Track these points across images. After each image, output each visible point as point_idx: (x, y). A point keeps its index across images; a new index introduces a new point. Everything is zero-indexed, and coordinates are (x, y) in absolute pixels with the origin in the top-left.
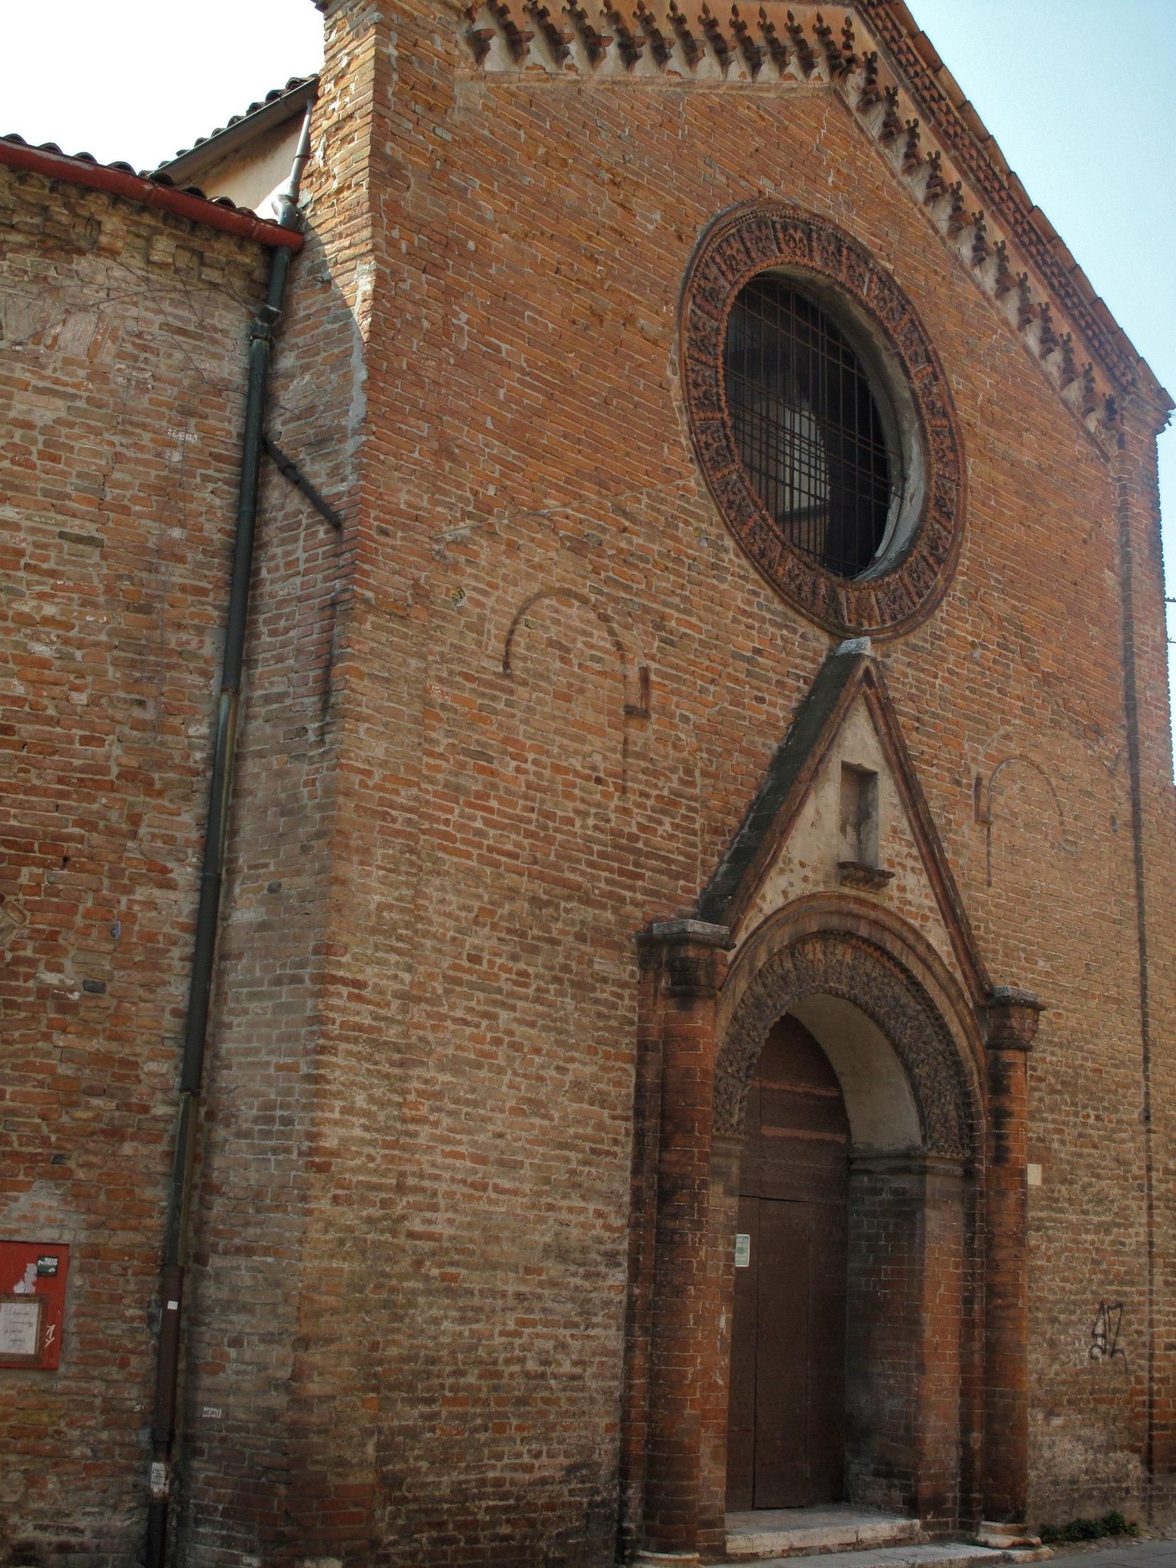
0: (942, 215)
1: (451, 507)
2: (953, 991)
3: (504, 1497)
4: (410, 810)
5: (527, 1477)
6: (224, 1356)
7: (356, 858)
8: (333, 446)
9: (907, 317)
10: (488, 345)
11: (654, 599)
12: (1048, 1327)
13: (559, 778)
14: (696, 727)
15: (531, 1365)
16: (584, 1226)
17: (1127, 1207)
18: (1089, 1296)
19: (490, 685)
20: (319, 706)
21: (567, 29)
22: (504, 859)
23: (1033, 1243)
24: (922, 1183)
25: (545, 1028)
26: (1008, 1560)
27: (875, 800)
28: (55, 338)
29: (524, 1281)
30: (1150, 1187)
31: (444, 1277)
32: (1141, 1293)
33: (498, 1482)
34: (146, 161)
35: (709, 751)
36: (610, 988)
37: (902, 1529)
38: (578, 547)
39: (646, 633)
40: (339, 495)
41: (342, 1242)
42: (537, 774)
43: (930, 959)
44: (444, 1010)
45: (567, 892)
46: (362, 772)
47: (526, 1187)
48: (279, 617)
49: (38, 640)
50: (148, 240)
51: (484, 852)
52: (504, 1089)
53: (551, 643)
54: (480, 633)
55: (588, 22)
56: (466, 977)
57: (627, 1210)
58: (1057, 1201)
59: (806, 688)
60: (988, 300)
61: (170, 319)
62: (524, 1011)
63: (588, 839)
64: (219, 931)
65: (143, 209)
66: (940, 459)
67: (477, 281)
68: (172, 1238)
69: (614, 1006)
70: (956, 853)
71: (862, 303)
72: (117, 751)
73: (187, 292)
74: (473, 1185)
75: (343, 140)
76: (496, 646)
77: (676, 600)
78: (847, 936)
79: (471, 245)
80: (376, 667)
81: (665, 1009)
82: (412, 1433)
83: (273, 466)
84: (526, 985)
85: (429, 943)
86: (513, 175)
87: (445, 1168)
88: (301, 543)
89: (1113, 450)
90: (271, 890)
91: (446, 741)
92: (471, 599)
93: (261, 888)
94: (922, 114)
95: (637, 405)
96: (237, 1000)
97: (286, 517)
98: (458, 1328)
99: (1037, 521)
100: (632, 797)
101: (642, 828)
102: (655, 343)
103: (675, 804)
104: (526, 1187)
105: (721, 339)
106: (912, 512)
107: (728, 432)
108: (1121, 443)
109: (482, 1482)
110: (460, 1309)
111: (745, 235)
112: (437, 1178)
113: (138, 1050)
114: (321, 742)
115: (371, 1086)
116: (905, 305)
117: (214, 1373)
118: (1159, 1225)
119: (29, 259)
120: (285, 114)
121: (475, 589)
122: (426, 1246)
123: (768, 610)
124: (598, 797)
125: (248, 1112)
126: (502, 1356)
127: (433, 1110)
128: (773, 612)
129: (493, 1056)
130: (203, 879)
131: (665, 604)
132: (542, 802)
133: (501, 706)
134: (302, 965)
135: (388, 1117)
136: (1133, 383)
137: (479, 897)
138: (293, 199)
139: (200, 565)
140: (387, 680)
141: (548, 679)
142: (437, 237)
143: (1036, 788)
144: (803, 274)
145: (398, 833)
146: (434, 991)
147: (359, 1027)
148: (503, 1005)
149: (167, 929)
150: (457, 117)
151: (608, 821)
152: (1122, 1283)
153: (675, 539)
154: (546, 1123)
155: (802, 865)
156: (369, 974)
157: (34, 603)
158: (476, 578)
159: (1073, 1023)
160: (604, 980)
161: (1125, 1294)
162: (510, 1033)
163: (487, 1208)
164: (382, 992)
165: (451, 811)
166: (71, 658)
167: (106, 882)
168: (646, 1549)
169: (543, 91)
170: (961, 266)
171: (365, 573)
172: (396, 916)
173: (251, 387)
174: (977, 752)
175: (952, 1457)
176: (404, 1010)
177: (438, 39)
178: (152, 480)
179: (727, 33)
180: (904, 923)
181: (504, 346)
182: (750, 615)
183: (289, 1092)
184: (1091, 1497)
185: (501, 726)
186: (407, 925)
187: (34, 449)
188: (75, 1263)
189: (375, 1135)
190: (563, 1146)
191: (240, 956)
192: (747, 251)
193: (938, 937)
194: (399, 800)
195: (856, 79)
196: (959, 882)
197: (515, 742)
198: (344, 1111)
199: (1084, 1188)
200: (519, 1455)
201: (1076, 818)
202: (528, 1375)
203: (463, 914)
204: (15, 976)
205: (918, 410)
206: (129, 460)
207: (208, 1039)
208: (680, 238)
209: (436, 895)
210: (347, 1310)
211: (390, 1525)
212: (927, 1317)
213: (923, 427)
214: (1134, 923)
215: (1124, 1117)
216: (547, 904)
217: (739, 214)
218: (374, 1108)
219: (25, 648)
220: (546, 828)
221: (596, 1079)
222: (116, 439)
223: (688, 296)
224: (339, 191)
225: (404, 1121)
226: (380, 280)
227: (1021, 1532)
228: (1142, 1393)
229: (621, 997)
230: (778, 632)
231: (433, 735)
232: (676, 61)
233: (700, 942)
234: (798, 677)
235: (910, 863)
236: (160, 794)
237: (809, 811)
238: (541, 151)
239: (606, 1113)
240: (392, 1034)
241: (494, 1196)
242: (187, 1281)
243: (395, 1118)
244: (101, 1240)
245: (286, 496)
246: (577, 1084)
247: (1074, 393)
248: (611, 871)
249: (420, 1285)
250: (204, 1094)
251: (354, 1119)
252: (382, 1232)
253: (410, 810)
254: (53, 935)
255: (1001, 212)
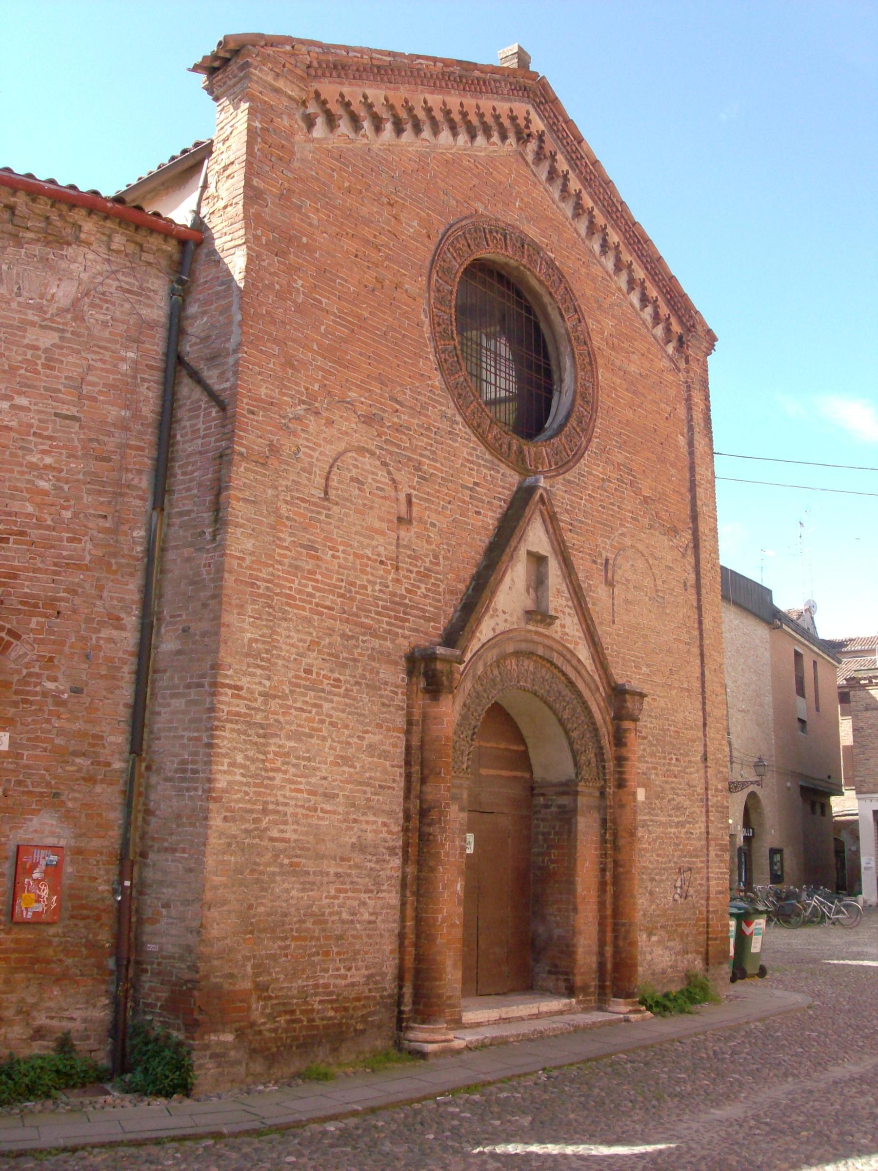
0: (582, 226)
1: (292, 397)
2: (593, 686)
3: (331, 993)
4: (268, 581)
5: (343, 982)
6: (160, 914)
7: (235, 611)
8: (221, 360)
9: (562, 286)
10: (315, 299)
11: (414, 451)
12: (649, 884)
13: (358, 562)
14: (440, 530)
15: (345, 916)
16: (375, 831)
17: (695, 812)
18: (672, 864)
19: (315, 504)
20: (213, 518)
21: (362, 113)
22: (325, 611)
23: (640, 834)
24: (575, 801)
25: (350, 713)
26: (627, 1020)
27: (547, 573)
28: (53, 295)
29: (341, 866)
30: (707, 800)
31: (291, 864)
32: (702, 862)
33: (326, 986)
34: (108, 191)
35: (447, 544)
36: (389, 688)
37: (565, 1005)
38: (369, 420)
39: (410, 473)
40: (225, 390)
41: (229, 845)
42: (344, 558)
43: (580, 667)
44: (290, 703)
45: (363, 630)
46: (239, 558)
47: (341, 809)
48: (187, 464)
49: (42, 478)
50: (110, 237)
51: (313, 606)
52: (327, 750)
53: (352, 479)
54: (310, 473)
55: (375, 109)
56: (303, 682)
57: (401, 821)
58: (654, 809)
59: (505, 506)
60: (610, 276)
61: (123, 284)
62: (338, 703)
63: (377, 598)
64: (152, 656)
65: (106, 218)
66: (583, 370)
67: (308, 261)
68: (125, 843)
69: (393, 699)
70: (594, 604)
71: (536, 277)
72: (89, 546)
73: (133, 268)
74: (308, 809)
75: (228, 177)
76: (320, 481)
77: (427, 453)
78: (530, 654)
79: (304, 240)
80: (247, 494)
81: (421, 700)
82: (274, 957)
83: (184, 372)
84: (339, 687)
85: (280, 662)
86: (329, 198)
87: (292, 798)
88: (201, 419)
89: (682, 365)
90: (184, 630)
91: (290, 539)
92: (304, 453)
93: (177, 630)
94: (571, 167)
95: (404, 336)
96: (164, 698)
97: (192, 403)
98: (301, 895)
99: (639, 406)
100: (402, 572)
101: (408, 591)
102: (414, 299)
103: (429, 577)
104: (341, 809)
105: (454, 297)
106: (566, 399)
107: (459, 352)
108: (687, 362)
109: (316, 986)
110: (302, 883)
111: (468, 236)
112: (286, 804)
113: (104, 729)
114: (214, 539)
115: (246, 750)
116: (562, 277)
117: (153, 924)
118: (712, 822)
119: (37, 249)
120: (191, 162)
121: (307, 447)
122: (280, 845)
123: (482, 459)
124: (382, 572)
125: (171, 765)
126: (327, 911)
127: (284, 763)
128: (486, 461)
129: (320, 730)
130: (143, 624)
131: (421, 455)
132: (348, 575)
133: (323, 518)
134: (203, 676)
135: (257, 768)
136: (694, 326)
137: (310, 634)
138: (197, 212)
139: (140, 432)
140: (254, 502)
141: (351, 501)
142: (284, 235)
143: (640, 564)
144: (502, 259)
145: (261, 596)
146: (283, 691)
147: (238, 714)
148: (326, 700)
149: (120, 654)
150: (296, 165)
151: (388, 587)
152: (691, 856)
153: (426, 416)
154: (352, 770)
155: (504, 612)
156: (244, 682)
157: (39, 456)
158: (307, 440)
159: (662, 704)
160: (386, 683)
161: (694, 863)
162: (330, 716)
163: (316, 822)
164: (252, 693)
165: (293, 582)
166: (61, 489)
167: (83, 626)
168: (415, 1022)
169: (348, 149)
170: (594, 255)
171: (241, 437)
172: (260, 646)
173: (171, 324)
174: (606, 543)
175: (593, 961)
176: (265, 703)
177: (285, 117)
178: (111, 381)
179: (457, 117)
180: (564, 646)
181: (324, 300)
182: (472, 462)
183: (196, 754)
184: (674, 981)
185: (322, 530)
186: (267, 651)
187: (39, 362)
188: (68, 859)
189: (249, 780)
190: (361, 783)
191: (165, 671)
192: (469, 246)
193: (583, 653)
194: (261, 575)
195: (532, 146)
196: (596, 621)
197: (331, 540)
198: (230, 765)
199: (669, 801)
200: (338, 969)
201: (663, 582)
202: (343, 922)
203: (301, 644)
204: (28, 684)
205: (570, 341)
206: (96, 369)
207: (146, 721)
208: (429, 237)
209: (285, 633)
210: (233, 886)
211: (262, 1013)
212: (579, 880)
213: (572, 350)
214: (698, 643)
215: (693, 759)
216: (352, 637)
217: (464, 223)
218: (248, 763)
219: (33, 484)
220: (350, 592)
221: (382, 743)
222: (89, 356)
223: (434, 271)
224: (225, 207)
225: (266, 770)
226: (250, 260)
227: (634, 1004)
228: (702, 920)
229: (396, 693)
230: (488, 473)
231: (282, 535)
232: (426, 134)
233: (445, 660)
234: (500, 499)
235: (567, 610)
236: (115, 572)
237: (507, 580)
238: (347, 184)
239: (388, 763)
240: (259, 718)
241: (321, 815)
242: (136, 868)
243: (261, 769)
244: (83, 845)
245: (192, 390)
246: (370, 746)
247: (659, 331)
248: (390, 617)
249: (277, 870)
250: (144, 755)
251: (236, 770)
252: (254, 838)
253: (268, 581)
254: (51, 659)
255: (617, 225)
